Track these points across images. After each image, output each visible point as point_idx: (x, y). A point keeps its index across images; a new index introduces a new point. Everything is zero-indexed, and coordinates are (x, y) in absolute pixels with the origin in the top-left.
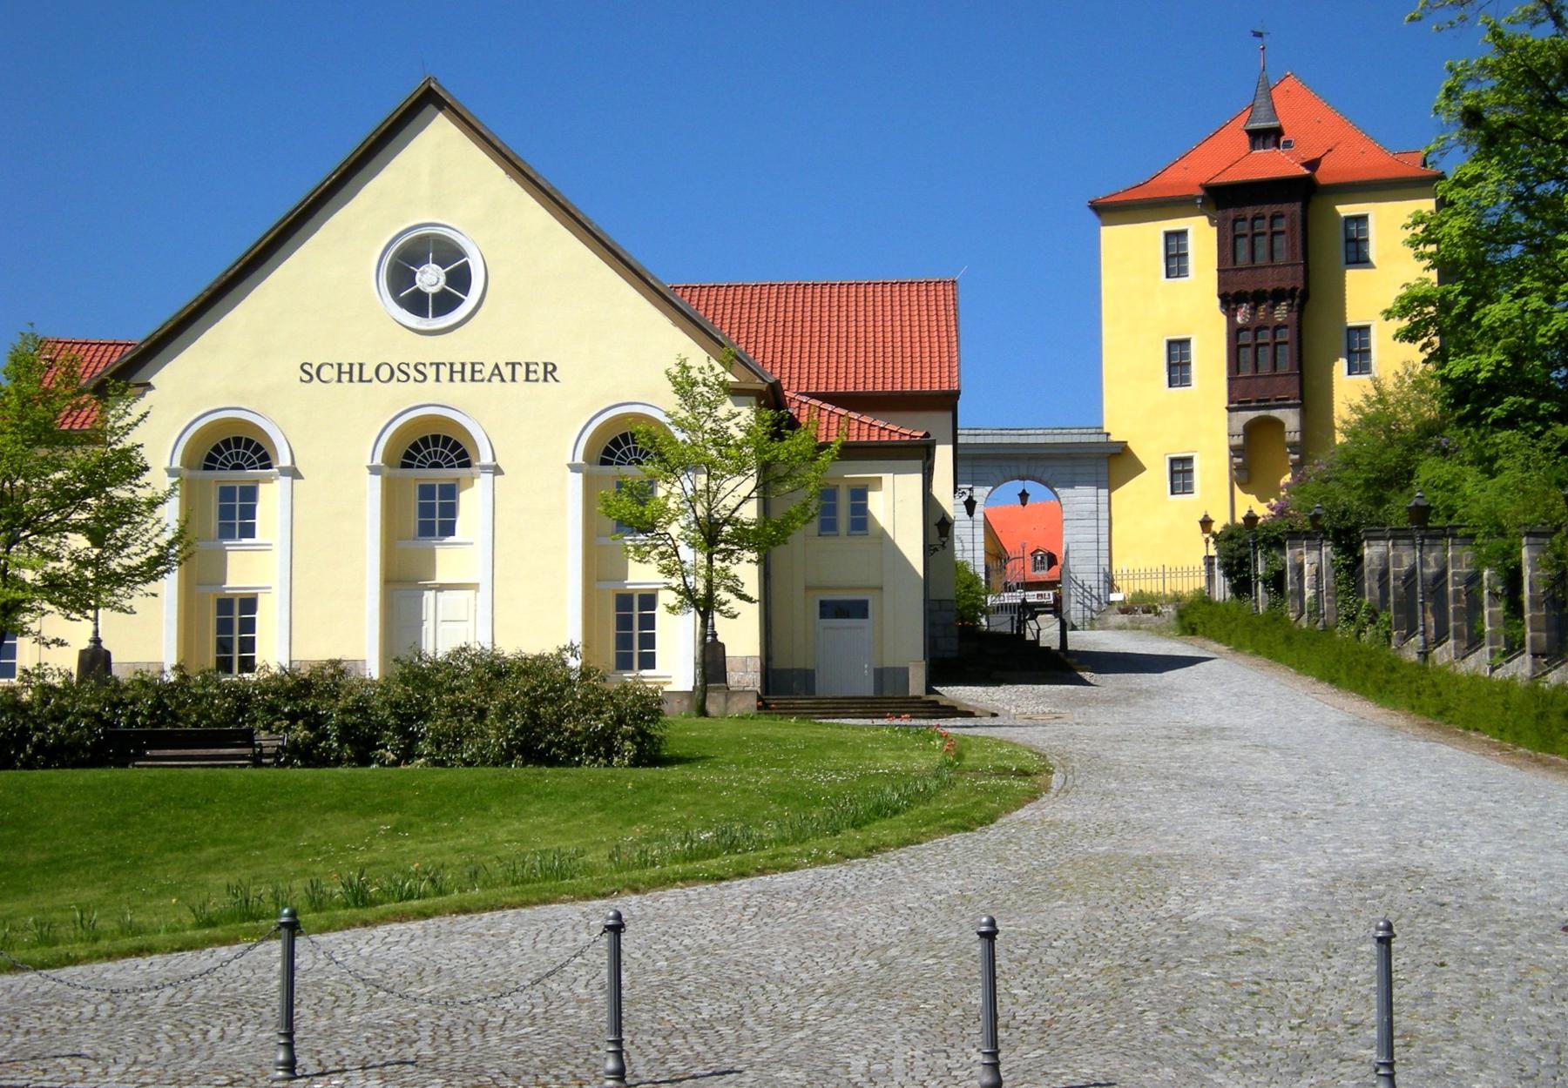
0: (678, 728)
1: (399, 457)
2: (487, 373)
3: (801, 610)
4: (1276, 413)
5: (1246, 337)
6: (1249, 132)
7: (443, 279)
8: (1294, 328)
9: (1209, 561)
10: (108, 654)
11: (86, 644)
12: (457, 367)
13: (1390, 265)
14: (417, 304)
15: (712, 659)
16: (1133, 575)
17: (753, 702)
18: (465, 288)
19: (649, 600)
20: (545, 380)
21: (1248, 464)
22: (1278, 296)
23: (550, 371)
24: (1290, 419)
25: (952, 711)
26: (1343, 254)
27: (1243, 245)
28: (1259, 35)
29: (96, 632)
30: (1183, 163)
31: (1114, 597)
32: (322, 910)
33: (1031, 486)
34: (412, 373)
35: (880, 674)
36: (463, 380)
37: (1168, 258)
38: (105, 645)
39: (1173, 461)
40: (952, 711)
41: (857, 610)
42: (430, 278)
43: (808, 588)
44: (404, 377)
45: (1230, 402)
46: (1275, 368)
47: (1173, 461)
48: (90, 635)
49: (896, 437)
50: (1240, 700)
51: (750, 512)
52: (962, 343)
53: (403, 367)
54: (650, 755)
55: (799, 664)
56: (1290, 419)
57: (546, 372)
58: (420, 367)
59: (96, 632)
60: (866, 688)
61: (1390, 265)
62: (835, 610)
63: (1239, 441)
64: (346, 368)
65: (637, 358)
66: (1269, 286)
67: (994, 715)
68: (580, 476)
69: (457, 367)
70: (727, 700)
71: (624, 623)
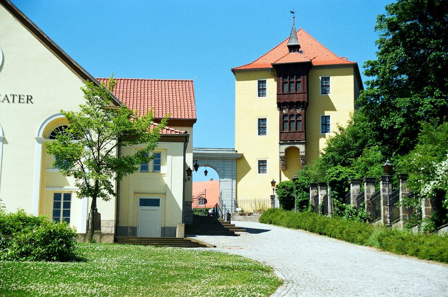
0: (80, 247)
4: (297, 146)
5: (287, 119)
6: (289, 47)
8: (303, 116)
9: (273, 197)
13: (342, 94)
15: (95, 221)
17: (112, 238)
19: (68, 196)
20: (27, 102)
21: (285, 163)
22: (298, 105)
23: (29, 99)
24: (302, 148)
25: (197, 245)
26: (321, 89)
27: (286, 87)
28: (293, 13)
30: (265, 57)
33: (209, 169)
35: (164, 229)
37: (259, 90)
39: (259, 161)
40: (197, 245)
41: (155, 203)
43: (135, 193)
45: (280, 141)
46: (297, 129)
47: (259, 161)
49: (173, 133)
51: (114, 154)
52: (196, 101)
54: (66, 256)
55: (131, 225)
56: (302, 148)
57: (28, 99)
60: (158, 235)
61: (342, 94)
62: (144, 202)
65: (69, 96)
66: (295, 100)
67: (215, 247)
68: (40, 146)
70: (101, 238)
71: (57, 205)
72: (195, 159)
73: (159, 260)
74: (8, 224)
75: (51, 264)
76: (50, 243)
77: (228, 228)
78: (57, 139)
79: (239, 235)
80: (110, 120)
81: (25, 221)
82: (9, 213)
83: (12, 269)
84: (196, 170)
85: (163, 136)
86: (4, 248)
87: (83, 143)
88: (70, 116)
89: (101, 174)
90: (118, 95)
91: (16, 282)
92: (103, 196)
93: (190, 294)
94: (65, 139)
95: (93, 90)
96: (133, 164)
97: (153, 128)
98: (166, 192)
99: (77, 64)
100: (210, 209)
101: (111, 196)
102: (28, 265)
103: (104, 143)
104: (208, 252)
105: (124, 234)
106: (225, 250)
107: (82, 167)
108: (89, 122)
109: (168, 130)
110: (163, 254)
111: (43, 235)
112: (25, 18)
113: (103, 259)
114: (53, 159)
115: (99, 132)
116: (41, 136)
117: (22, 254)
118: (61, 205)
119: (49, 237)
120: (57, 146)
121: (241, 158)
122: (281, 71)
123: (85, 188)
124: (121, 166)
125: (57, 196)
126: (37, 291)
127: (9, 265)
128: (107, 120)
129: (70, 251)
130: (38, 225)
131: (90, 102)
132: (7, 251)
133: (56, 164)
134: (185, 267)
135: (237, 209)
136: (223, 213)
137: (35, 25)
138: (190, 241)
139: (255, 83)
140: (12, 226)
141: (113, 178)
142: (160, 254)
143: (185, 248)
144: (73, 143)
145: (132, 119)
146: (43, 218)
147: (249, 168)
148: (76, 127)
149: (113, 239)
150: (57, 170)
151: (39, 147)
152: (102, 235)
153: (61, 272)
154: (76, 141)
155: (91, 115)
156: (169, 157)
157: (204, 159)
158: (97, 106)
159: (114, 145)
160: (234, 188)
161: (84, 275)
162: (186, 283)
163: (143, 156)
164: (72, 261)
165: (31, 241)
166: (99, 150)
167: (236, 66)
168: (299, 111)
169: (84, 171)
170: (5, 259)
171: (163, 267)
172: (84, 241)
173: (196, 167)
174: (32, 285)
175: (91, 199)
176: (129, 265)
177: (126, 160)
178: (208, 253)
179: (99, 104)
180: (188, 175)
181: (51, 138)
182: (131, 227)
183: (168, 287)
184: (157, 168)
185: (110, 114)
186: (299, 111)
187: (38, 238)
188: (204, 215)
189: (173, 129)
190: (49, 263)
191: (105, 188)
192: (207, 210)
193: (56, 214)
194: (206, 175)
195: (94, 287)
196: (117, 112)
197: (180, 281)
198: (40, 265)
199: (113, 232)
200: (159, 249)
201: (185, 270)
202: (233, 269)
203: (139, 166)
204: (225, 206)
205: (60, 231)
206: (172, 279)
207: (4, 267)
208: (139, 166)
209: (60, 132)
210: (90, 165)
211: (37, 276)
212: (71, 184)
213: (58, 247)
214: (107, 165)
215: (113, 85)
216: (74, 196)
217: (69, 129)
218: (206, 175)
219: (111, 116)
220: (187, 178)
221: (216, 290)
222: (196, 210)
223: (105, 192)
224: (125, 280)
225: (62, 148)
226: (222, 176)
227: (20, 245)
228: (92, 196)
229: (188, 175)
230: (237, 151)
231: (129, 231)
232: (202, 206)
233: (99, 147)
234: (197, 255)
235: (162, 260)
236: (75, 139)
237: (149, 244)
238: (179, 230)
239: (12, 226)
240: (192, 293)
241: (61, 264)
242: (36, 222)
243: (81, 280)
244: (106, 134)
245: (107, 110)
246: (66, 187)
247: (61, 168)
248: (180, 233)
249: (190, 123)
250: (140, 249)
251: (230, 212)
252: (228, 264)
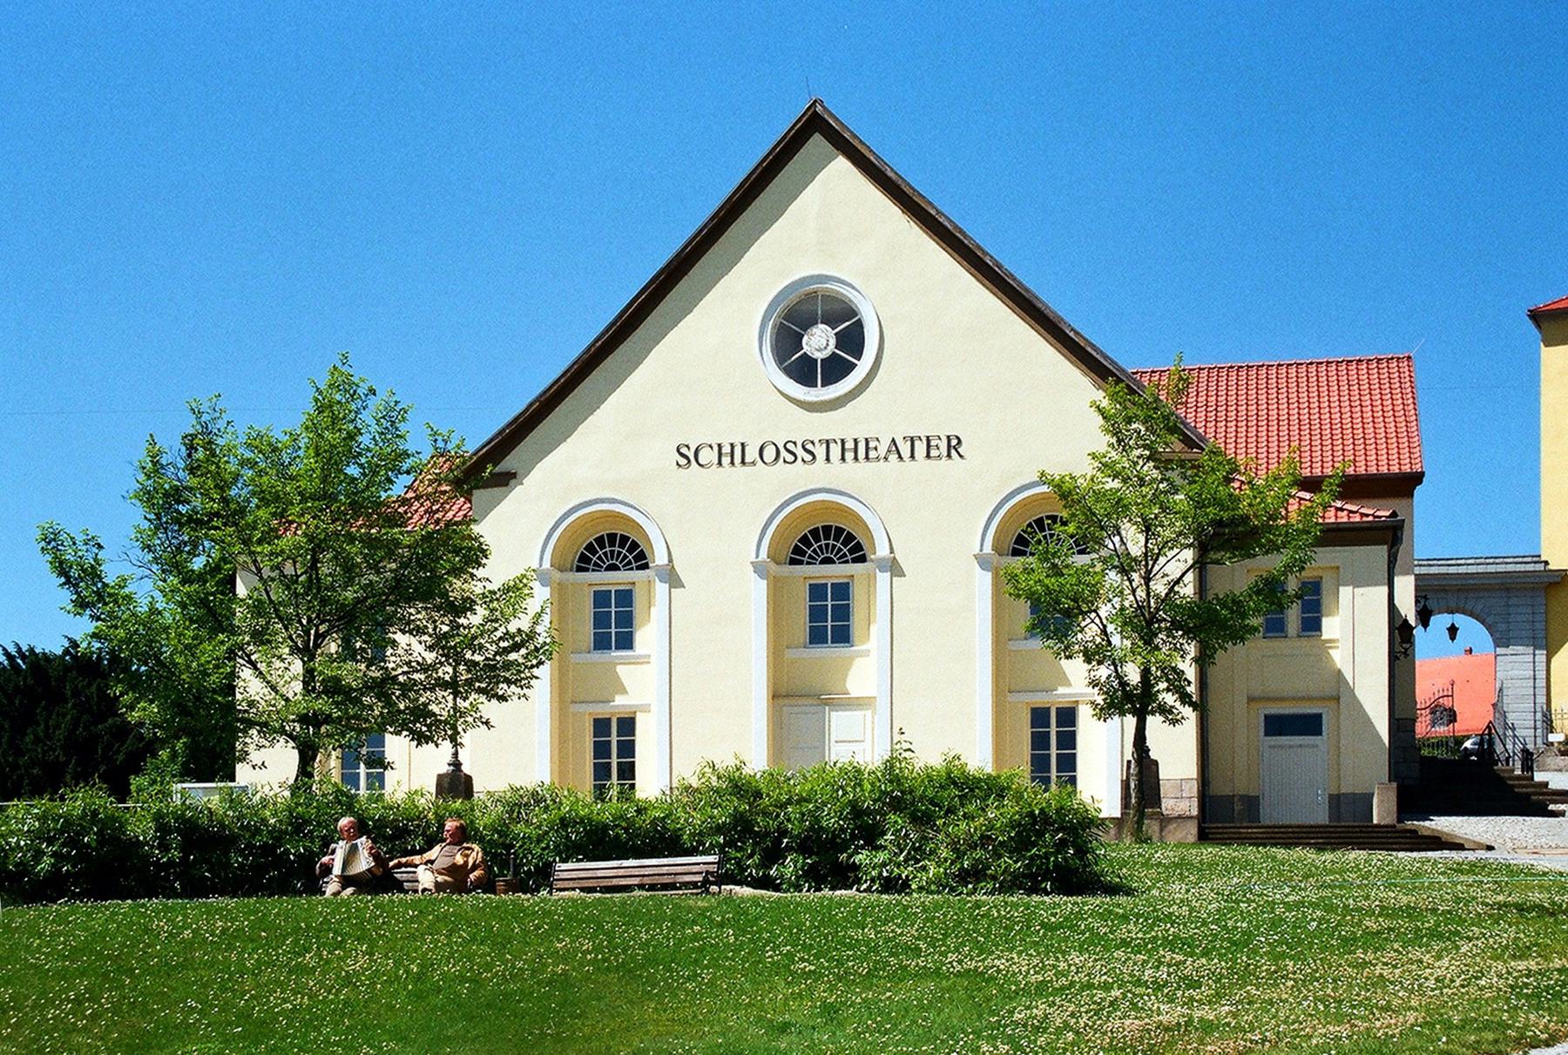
0: (1113, 853)
1: (787, 552)
2: (882, 451)
3: (1242, 727)
7: (833, 342)
10: (469, 779)
11: (445, 769)
12: (850, 445)
14: (804, 371)
15: (1143, 778)
17: (1192, 830)
18: (858, 352)
19: (1068, 716)
20: (949, 456)
23: (954, 445)
29: (456, 754)
33: (1460, 620)
34: (800, 452)
35: (1336, 801)
36: (856, 458)
38: (466, 769)
41: (1310, 725)
42: (819, 341)
43: (1251, 699)
44: (790, 458)
48: (449, 758)
49: (1356, 518)
51: (1188, 590)
53: (790, 446)
54: (1077, 878)
58: (810, 447)
59: (456, 754)
60: (1322, 817)
62: (1278, 725)
65: (1057, 428)
67: (1490, 848)
68: (988, 576)
69: (850, 445)
72: (1421, 596)
73: (1332, 887)
74: (922, 798)
75: (1043, 903)
76: (1034, 844)
77: (1528, 795)
78: (1032, 554)
79: (1562, 814)
80: (1176, 493)
81: (963, 788)
82: (922, 764)
83: (945, 915)
84: (1425, 624)
85: (1329, 530)
86: (917, 861)
87: (1104, 561)
88: (1065, 487)
89: (1157, 648)
90: (1194, 417)
91: (956, 949)
92: (1165, 710)
93: (1431, 983)
94: (1054, 555)
95: (1125, 408)
96: (1244, 616)
97: (1298, 505)
98: (1339, 691)
99: (1077, 333)
100: (1468, 737)
101: (1188, 711)
102: (985, 904)
103: (1162, 560)
104: (1473, 865)
105: (1225, 816)
106: (1522, 859)
107: (1104, 631)
108: (1120, 500)
109: (1342, 509)
110: (1341, 872)
111: (1013, 824)
112: (933, 212)
113: (1176, 887)
114: (1022, 612)
115: (1147, 528)
116: (988, 549)
117: (964, 877)
118: (1052, 737)
119: (1031, 828)
120: (1035, 577)
123: (1116, 691)
124: (1210, 623)
125: (1039, 716)
126: (1014, 974)
127: (937, 906)
128: (1166, 493)
129: (1085, 866)
130: (1001, 796)
131: (1119, 441)
132: (924, 868)
133: (1034, 626)
134: (1408, 906)
135: (1552, 738)
136: (1507, 748)
137: (961, 231)
138: (1415, 832)
140: (932, 802)
141: (1189, 657)
142: (1332, 872)
143: (1401, 854)
144: (1078, 565)
145: (1236, 485)
146: (1010, 778)
148: (1082, 518)
149: (1194, 831)
150: (1036, 644)
151: (983, 582)
152: (1165, 821)
153: (1070, 923)
154: (1082, 560)
155: (1124, 481)
156: (1345, 592)
157: (1445, 591)
158: (1137, 452)
159: (1190, 562)
160: (1542, 674)
161: (1132, 930)
162: (1416, 953)
163: (1273, 591)
164: (1094, 894)
165: (985, 839)
166: (1147, 579)
169: (1109, 643)
170: (921, 889)
171: (1346, 907)
172: (1119, 836)
173: (1424, 616)
174: (999, 958)
175: (1131, 721)
176: (1249, 901)
177: (1224, 606)
178: (1473, 868)
179: (1145, 447)
180: (1403, 642)
181: (1016, 553)
182: (1242, 797)
183: (1365, 964)
184: (1312, 625)
185: (1174, 475)
187: (1002, 832)
188: (1449, 756)
189: (1354, 508)
190: (1036, 898)
191: (1168, 690)
192: (1459, 741)
193: (1040, 765)
194: (1453, 638)
195: (1161, 963)
196: (1194, 467)
197: (1396, 946)
198: (1015, 906)
199: (1195, 812)
200: (1328, 856)
201: (1409, 916)
202: (1552, 914)
203: (1261, 620)
204: (1513, 729)
205: (1058, 811)
206: (1375, 940)
207: (924, 911)
208: (1261, 620)
209: (1040, 536)
210: (1125, 624)
211: (1008, 935)
212: (1077, 680)
213: (1054, 855)
214: (1172, 623)
215: (1183, 383)
216: (1085, 715)
217: (1064, 524)
218: (1453, 638)
219: (1179, 481)
220: (1398, 648)
221: (1508, 973)
222: (1426, 742)
223: (1170, 699)
224: (1244, 942)
225: (1047, 581)
226: (1502, 640)
227: (955, 850)
228: (1134, 712)
229: (1403, 642)
230: (1546, 563)
231: (1238, 807)
232: (1442, 730)
233: (1149, 572)
234: (1443, 873)
235: (1341, 887)
236: (1081, 552)
237: (1297, 845)
238: (1381, 801)
239: (932, 802)
240: (1437, 980)
241: (1068, 903)
242: (991, 788)
243: (1125, 943)
244: (1168, 533)
245: (1163, 463)
246: (1061, 690)
247: (1049, 638)
248: (1382, 811)
249: (1404, 485)
250: (1274, 859)
251: (1530, 747)
252: (1536, 897)
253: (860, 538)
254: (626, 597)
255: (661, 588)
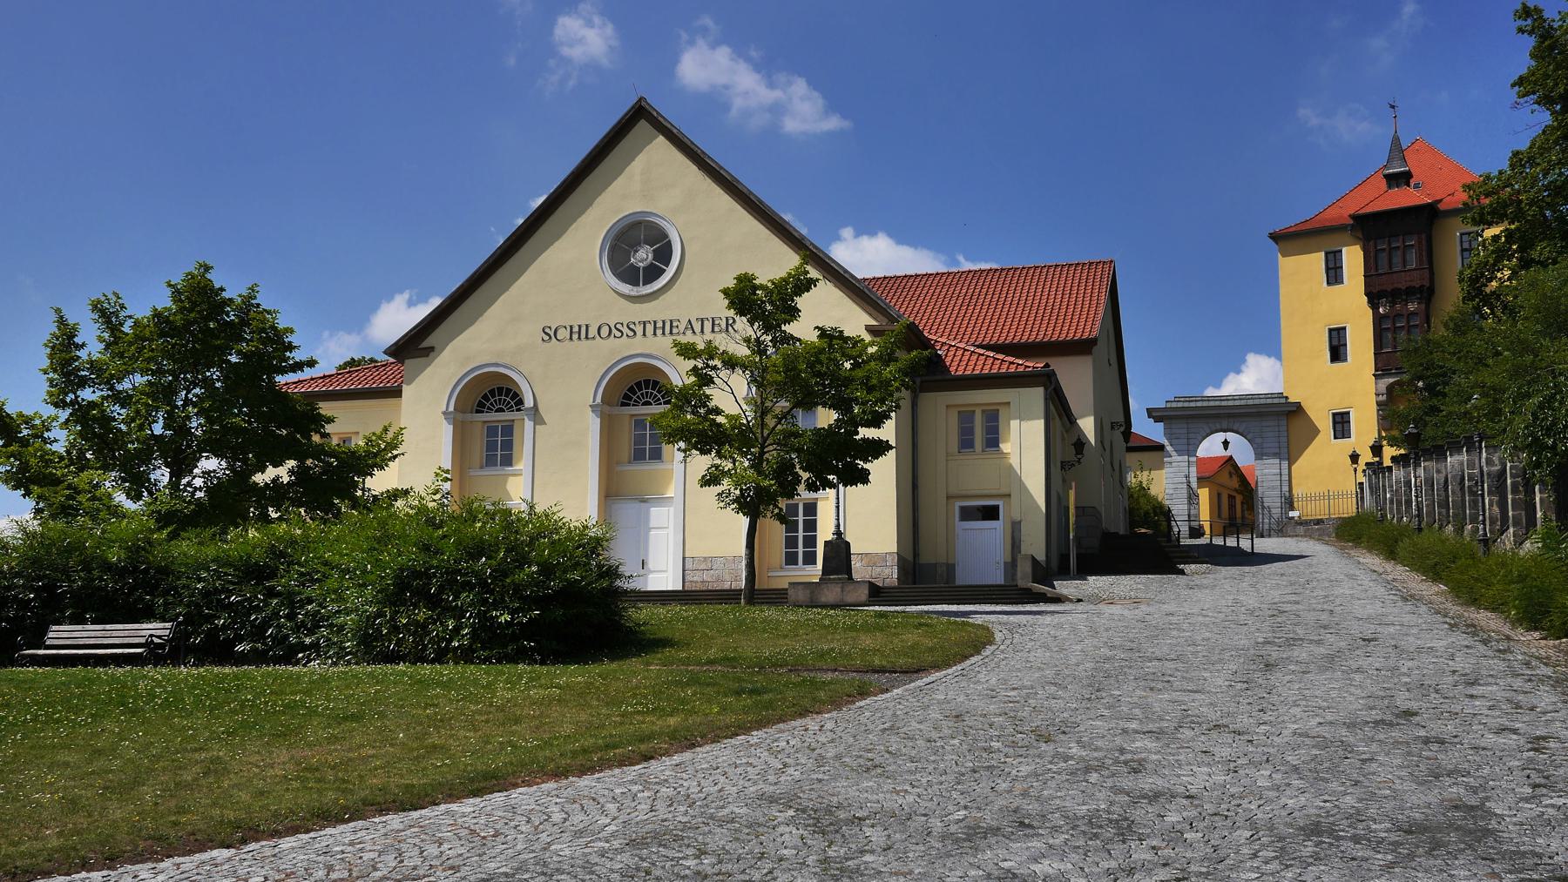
14: (630, 275)
16: (1310, 498)
22: (1410, 293)
27: (1384, 257)
31: (1291, 514)
32: (407, 786)
33: (1230, 436)
34: (625, 330)
37: (1328, 269)
50: (1360, 586)
62: (968, 514)
63: (1381, 398)
64: (576, 329)
66: (1403, 286)
69: (660, 324)
121: (1296, 411)
122: (1372, 228)
139: (1317, 260)
147: (1316, 432)
156: (1014, 424)
167: (1278, 228)
168: (1412, 307)
181: (623, 404)
184: (993, 441)
186: (1412, 307)
253: (514, 389)
254: (508, 430)
255: (529, 424)
